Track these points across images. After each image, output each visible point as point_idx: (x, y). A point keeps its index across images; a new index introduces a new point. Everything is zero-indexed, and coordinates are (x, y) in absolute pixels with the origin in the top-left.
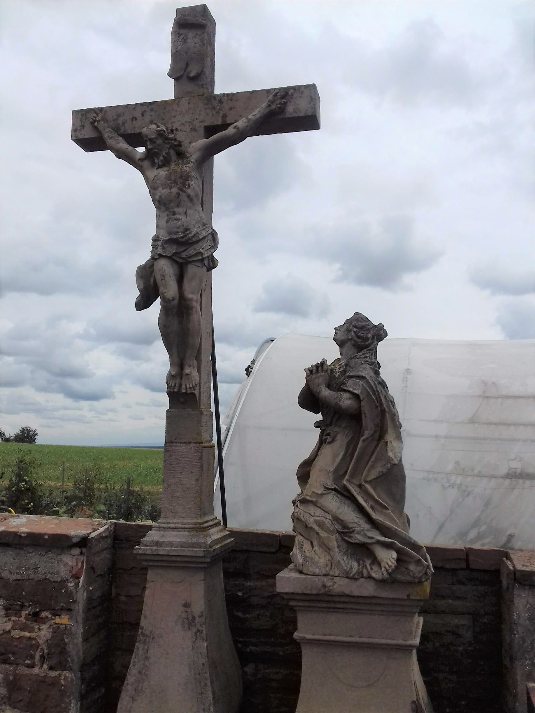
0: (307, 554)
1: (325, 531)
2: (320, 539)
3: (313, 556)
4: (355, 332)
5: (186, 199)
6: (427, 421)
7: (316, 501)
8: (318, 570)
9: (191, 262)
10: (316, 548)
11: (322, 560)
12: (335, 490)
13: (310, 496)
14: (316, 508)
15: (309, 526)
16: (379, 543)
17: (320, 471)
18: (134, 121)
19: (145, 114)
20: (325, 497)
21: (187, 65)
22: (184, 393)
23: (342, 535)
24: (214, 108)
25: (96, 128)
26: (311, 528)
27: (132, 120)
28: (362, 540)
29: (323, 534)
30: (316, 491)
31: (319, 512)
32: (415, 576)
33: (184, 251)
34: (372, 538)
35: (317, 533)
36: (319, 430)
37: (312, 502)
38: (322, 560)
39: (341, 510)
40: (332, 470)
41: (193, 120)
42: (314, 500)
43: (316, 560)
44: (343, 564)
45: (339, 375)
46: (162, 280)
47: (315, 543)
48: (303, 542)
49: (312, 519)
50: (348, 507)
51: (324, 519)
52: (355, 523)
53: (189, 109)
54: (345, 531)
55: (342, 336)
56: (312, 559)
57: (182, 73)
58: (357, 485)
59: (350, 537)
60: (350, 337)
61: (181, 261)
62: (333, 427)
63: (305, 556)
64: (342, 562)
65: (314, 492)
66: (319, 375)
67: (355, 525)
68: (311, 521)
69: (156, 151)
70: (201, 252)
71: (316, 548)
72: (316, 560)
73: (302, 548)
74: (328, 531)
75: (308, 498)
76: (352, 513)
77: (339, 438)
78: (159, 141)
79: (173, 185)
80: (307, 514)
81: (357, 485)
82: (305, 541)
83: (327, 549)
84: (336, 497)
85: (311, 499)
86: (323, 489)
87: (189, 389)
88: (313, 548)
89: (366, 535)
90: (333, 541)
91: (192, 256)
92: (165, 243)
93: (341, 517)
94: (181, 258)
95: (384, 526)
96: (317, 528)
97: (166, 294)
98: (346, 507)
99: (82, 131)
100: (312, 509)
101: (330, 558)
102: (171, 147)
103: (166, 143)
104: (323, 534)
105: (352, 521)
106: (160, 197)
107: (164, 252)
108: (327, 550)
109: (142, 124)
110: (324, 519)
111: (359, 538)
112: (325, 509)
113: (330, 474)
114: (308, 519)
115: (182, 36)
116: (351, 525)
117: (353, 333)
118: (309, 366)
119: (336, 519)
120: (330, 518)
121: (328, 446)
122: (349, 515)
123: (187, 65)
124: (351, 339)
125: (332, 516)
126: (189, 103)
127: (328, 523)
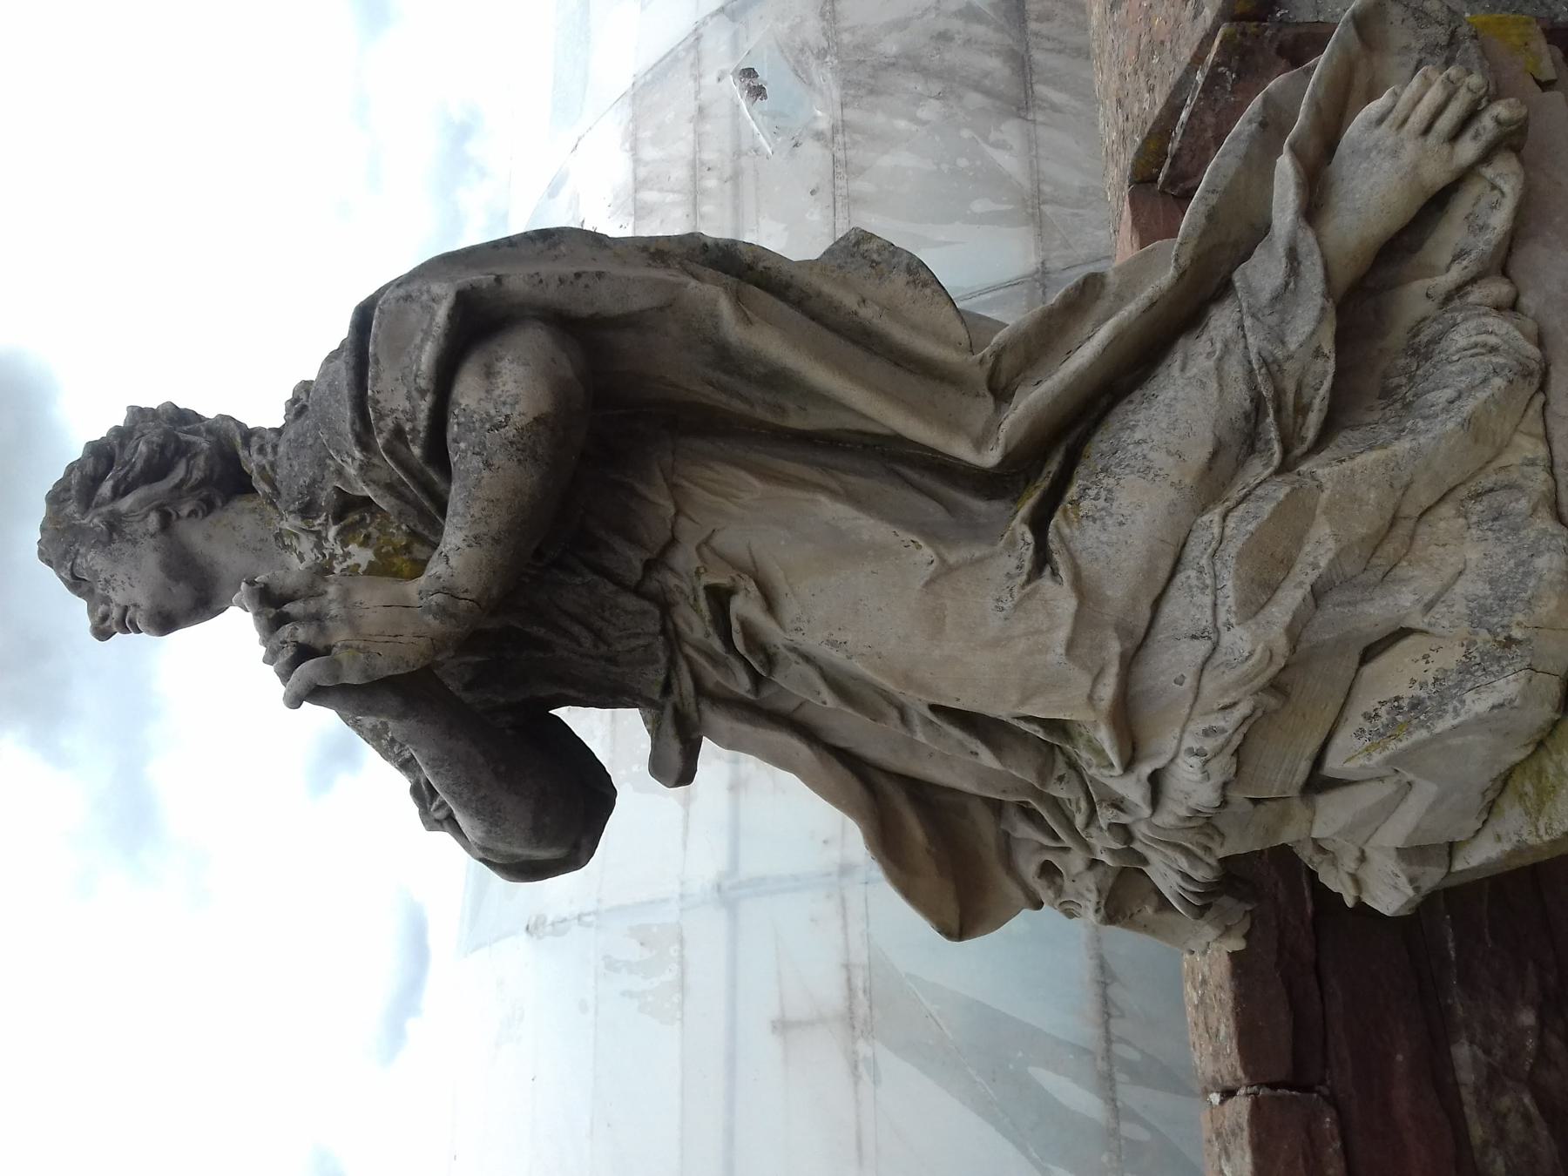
0: (1451, 657)
1: (1299, 540)
2: (1348, 581)
3: (1461, 608)
4: (118, 493)
7: (1123, 631)
8: (1541, 563)
10: (1401, 602)
11: (1473, 555)
12: (1039, 523)
13: (1096, 679)
14: (1161, 634)
15: (1281, 645)
16: (1313, 208)
17: (935, 624)
20: (1089, 568)
23: (1298, 452)
26: (1294, 634)
28: (1319, 301)
29: (1320, 549)
30: (1063, 634)
31: (1186, 608)
32: (1443, 40)
34: (1293, 255)
35: (1318, 594)
36: (712, 758)
37: (1130, 662)
38: (1473, 555)
39: (1159, 459)
40: (927, 552)
42: (1114, 647)
43: (1482, 589)
44: (1482, 395)
45: (365, 544)
47: (1376, 612)
48: (1371, 717)
49: (1239, 640)
50: (1133, 428)
51: (1232, 548)
52: (1219, 368)
54: (1270, 430)
55: (137, 576)
56: (1479, 615)
58: (998, 410)
59: (1302, 410)
60: (154, 519)
62: (672, 581)
63: (1465, 669)
64: (1469, 405)
65: (1071, 645)
66: (334, 610)
67: (1235, 369)
68: (1250, 643)
71: (1401, 602)
72: (1482, 589)
73: (1416, 704)
74: (1294, 517)
75: (1107, 690)
76: (1166, 396)
77: (732, 540)
80: (1209, 686)
81: (998, 410)
82: (1365, 701)
83: (1388, 540)
84: (1086, 504)
85: (1113, 670)
86: (1046, 582)
88: (1403, 633)
89: (1276, 298)
90: (1352, 474)
93: (1199, 454)
95: (1204, 234)
96: (1291, 597)
98: (1138, 436)
100: (1174, 660)
101: (1447, 510)
104: (1320, 549)
105: (1213, 386)
108: (1402, 530)
110: (1232, 548)
111: (1308, 320)
112: (1165, 564)
113: (952, 558)
114: (1230, 676)
116: (1239, 395)
117: (126, 504)
118: (270, 684)
119: (1215, 482)
120: (1214, 516)
121: (790, 609)
122: (1184, 406)
124: (166, 522)
125: (1204, 509)
127: (1242, 526)
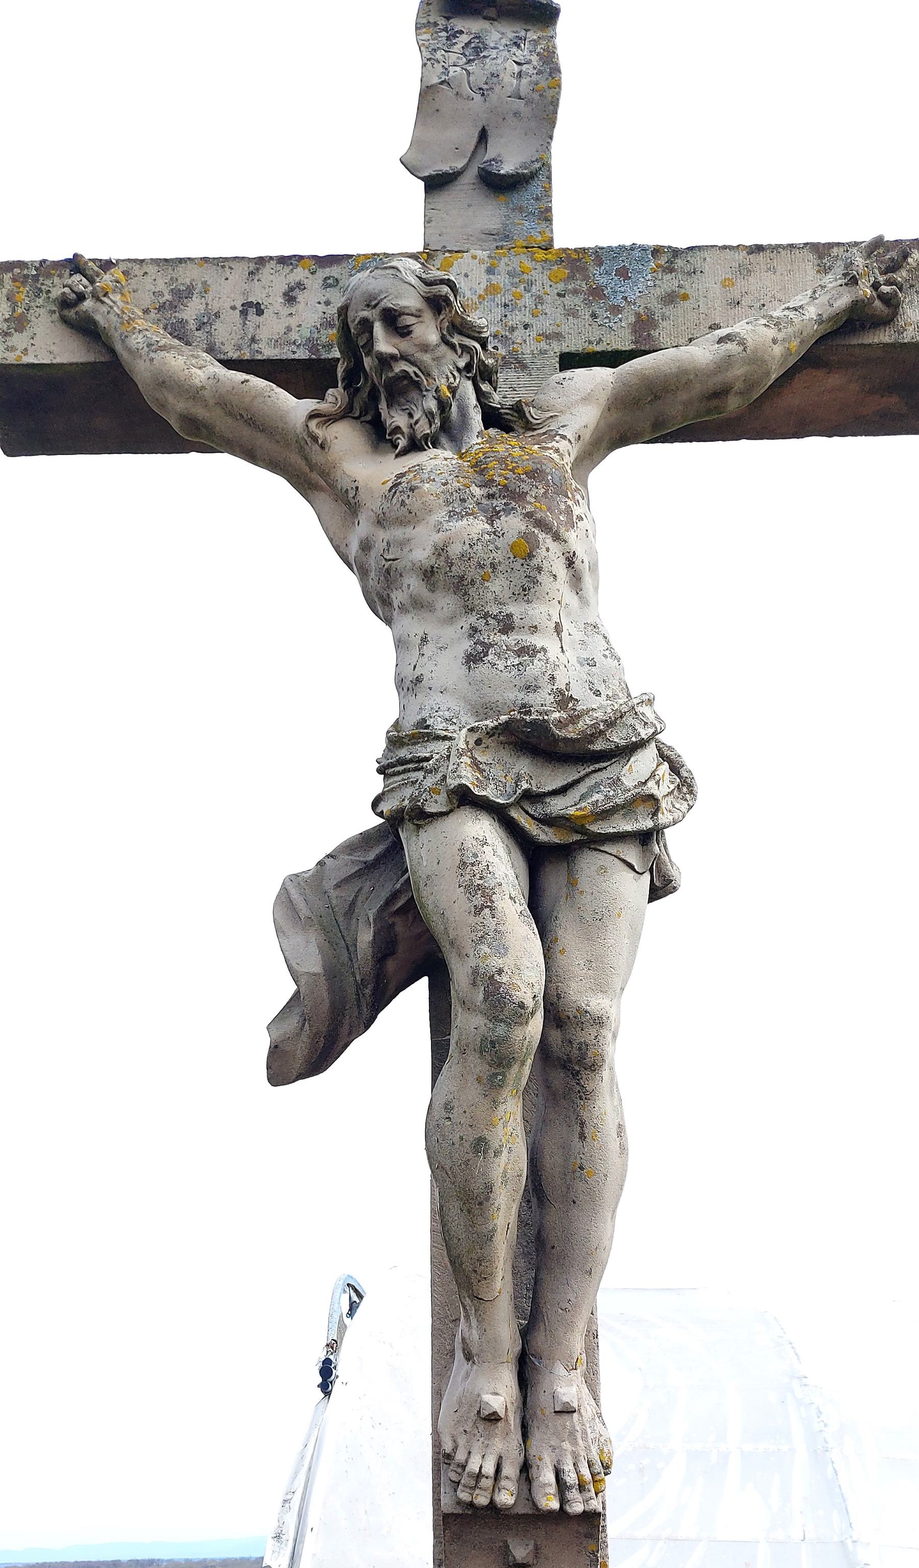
5: (559, 568)
6: (292, 1558)
9: (596, 842)
18: (252, 316)
19: (301, 297)
21: (483, 136)
22: (551, 1512)
24: (597, 293)
25: (87, 330)
27: (244, 313)
33: (562, 791)
41: (513, 329)
46: (478, 910)
53: (492, 289)
57: (459, 165)
61: (545, 835)
69: (411, 369)
70: (652, 797)
78: (428, 331)
79: (499, 503)
87: (573, 1495)
91: (605, 815)
92: (478, 742)
94: (547, 821)
97: (504, 979)
99: (17, 336)
102: (468, 367)
103: (452, 347)
106: (441, 550)
107: (480, 785)
109: (289, 329)
115: (464, 38)
123: (483, 136)
126: (490, 271)
